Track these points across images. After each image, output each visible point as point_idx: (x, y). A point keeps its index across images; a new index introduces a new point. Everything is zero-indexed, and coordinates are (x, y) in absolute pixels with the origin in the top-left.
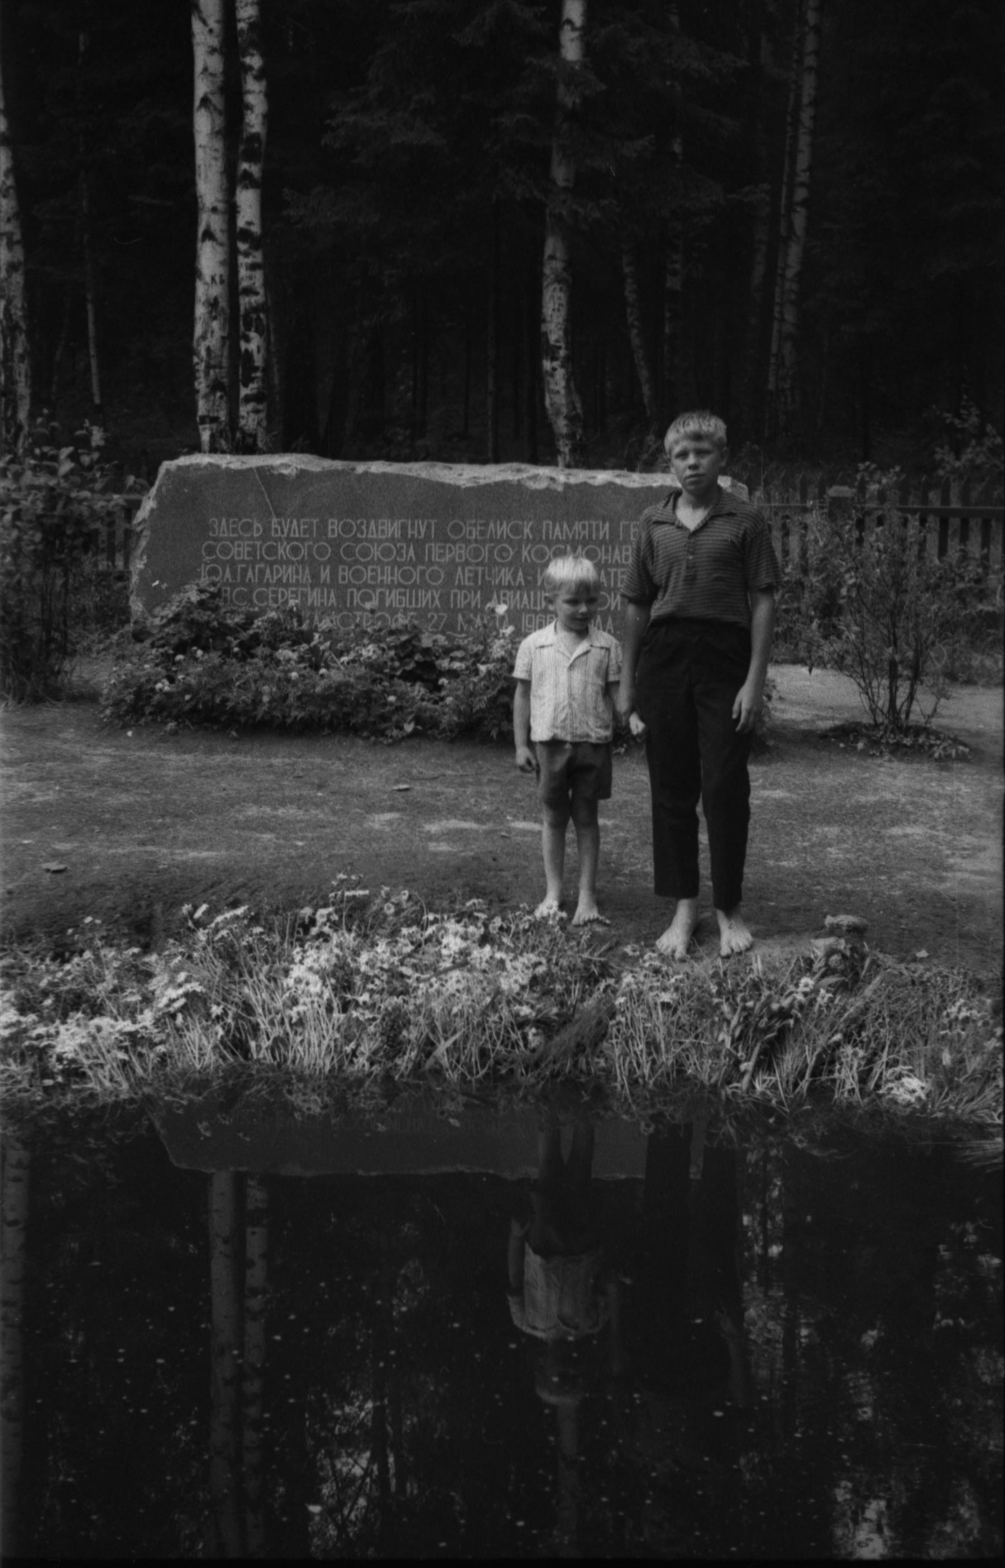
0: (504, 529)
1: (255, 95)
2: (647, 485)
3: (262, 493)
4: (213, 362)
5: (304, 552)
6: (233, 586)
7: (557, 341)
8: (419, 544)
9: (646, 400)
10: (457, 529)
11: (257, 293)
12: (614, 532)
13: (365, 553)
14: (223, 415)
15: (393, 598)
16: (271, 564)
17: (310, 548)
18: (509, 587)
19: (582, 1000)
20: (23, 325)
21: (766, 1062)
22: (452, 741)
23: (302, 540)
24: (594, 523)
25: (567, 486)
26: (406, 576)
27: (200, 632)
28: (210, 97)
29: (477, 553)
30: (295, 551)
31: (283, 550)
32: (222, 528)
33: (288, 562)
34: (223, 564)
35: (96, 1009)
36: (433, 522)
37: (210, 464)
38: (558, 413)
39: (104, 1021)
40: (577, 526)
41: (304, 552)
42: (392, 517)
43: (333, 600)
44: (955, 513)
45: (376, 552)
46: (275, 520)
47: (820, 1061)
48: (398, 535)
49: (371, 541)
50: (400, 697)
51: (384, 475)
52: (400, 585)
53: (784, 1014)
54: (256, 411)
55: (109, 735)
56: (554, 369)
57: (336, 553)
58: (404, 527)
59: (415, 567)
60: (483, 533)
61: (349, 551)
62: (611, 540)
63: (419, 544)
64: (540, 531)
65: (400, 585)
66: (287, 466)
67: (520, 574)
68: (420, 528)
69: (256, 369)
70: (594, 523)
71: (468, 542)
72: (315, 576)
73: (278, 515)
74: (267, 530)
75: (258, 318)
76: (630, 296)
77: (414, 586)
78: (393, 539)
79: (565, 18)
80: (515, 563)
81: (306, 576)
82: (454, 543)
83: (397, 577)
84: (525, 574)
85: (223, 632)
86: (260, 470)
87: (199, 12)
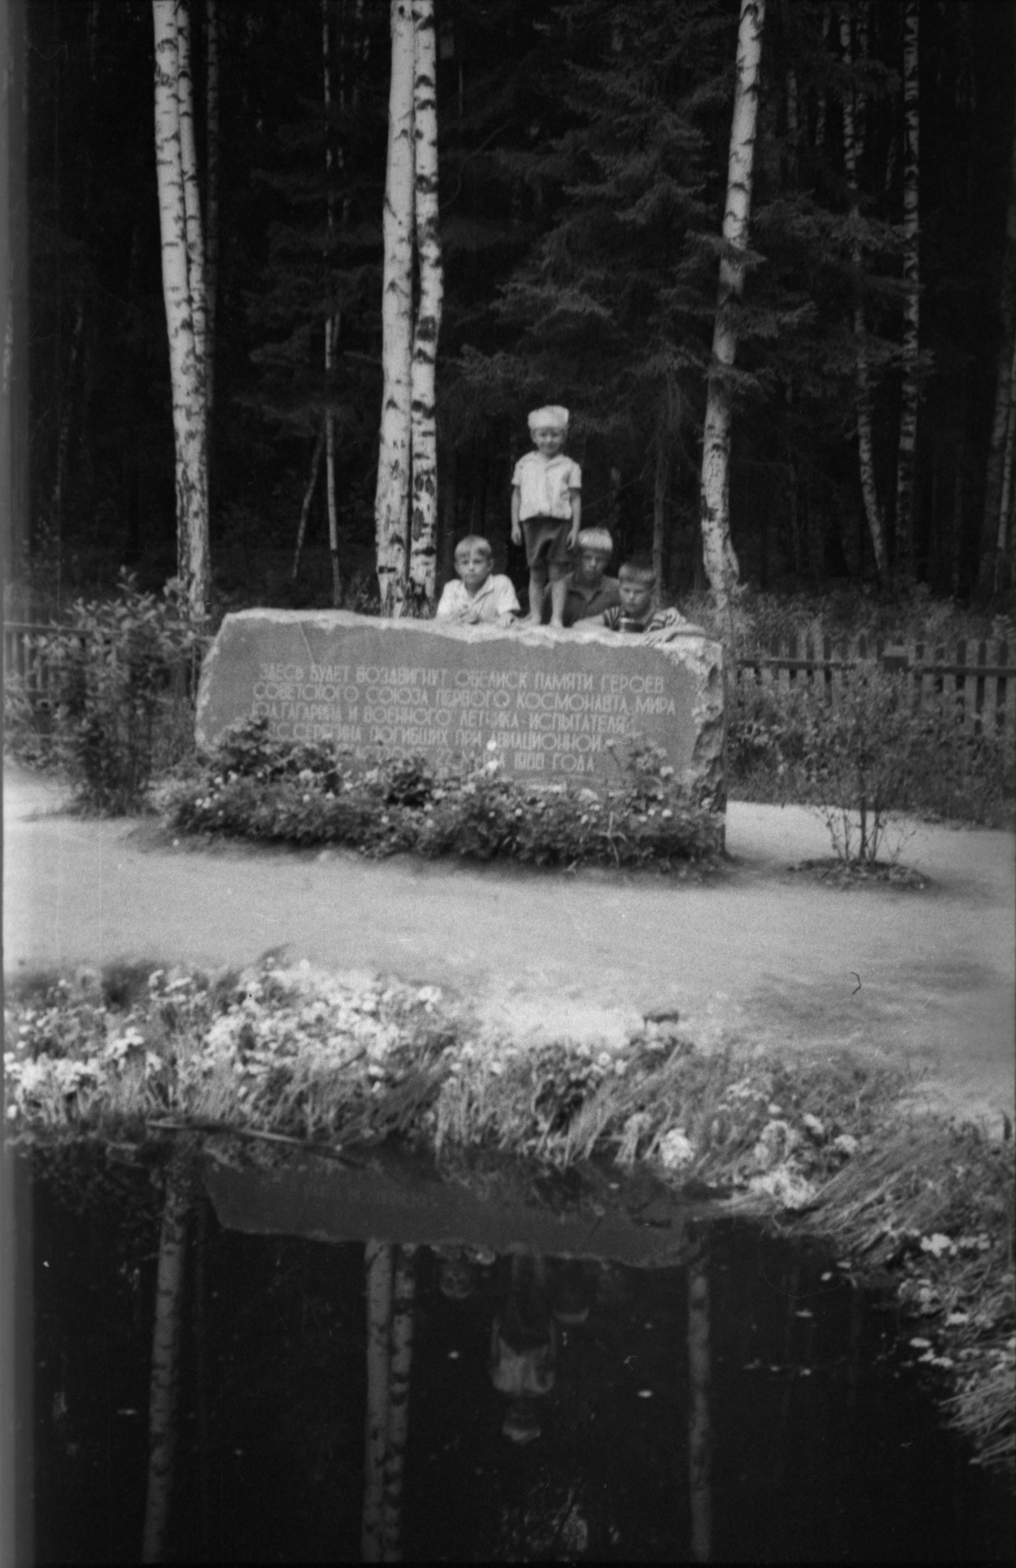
0: (504, 678)
1: (432, 280)
2: (626, 644)
3: (304, 645)
4: (392, 518)
5: (337, 694)
6: (278, 722)
7: (715, 504)
8: (431, 690)
9: (877, 554)
10: (463, 678)
11: (428, 458)
12: (596, 684)
13: (387, 696)
14: (400, 566)
15: (408, 735)
16: (310, 704)
17: (342, 691)
18: (506, 729)
19: (431, 1065)
20: (198, 486)
21: (562, 1122)
22: (434, 858)
23: (335, 684)
24: (580, 676)
25: (558, 644)
26: (420, 717)
27: (243, 759)
28: (398, 281)
29: (479, 699)
30: (330, 692)
31: (320, 693)
32: (271, 672)
33: (323, 702)
34: (270, 702)
35: (59, 1053)
36: (444, 671)
37: (264, 619)
38: (714, 570)
39: (62, 1064)
40: (565, 678)
41: (337, 694)
42: (410, 665)
43: (359, 737)
44: (992, 673)
45: (395, 696)
46: (313, 666)
47: (610, 1123)
48: (414, 681)
49: (392, 687)
50: (392, 818)
51: (406, 632)
52: (413, 725)
53: (580, 1084)
54: (427, 564)
55: (577, 867)
56: (711, 530)
57: (363, 697)
58: (419, 675)
59: (427, 709)
60: (485, 682)
61: (374, 695)
62: (595, 691)
63: (431, 690)
64: (533, 682)
65: (413, 725)
66: (325, 621)
67: (515, 718)
68: (432, 677)
69: (426, 525)
70: (580, 676)
71: (472, 689)
72: (345, 715)
73: (317, 662)
74: (307, 673)
75: (429, 480)
76: (865, 456)
77: (426, 726)
78: (409, 685)
79: (728, 210)
80: (511, 709)
81: (337, 715)
82: (461, 689)
83: (412, 717)
84: (519, 717)
85: (260, 759)
86: (304, 624)
87: (389, 205)
